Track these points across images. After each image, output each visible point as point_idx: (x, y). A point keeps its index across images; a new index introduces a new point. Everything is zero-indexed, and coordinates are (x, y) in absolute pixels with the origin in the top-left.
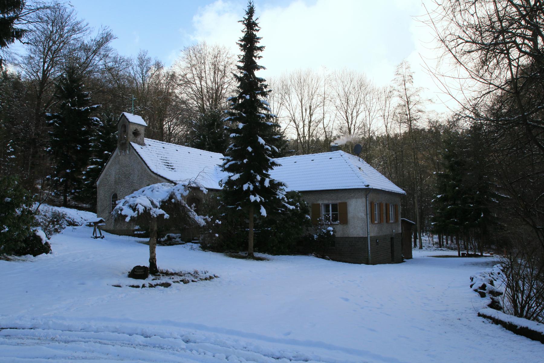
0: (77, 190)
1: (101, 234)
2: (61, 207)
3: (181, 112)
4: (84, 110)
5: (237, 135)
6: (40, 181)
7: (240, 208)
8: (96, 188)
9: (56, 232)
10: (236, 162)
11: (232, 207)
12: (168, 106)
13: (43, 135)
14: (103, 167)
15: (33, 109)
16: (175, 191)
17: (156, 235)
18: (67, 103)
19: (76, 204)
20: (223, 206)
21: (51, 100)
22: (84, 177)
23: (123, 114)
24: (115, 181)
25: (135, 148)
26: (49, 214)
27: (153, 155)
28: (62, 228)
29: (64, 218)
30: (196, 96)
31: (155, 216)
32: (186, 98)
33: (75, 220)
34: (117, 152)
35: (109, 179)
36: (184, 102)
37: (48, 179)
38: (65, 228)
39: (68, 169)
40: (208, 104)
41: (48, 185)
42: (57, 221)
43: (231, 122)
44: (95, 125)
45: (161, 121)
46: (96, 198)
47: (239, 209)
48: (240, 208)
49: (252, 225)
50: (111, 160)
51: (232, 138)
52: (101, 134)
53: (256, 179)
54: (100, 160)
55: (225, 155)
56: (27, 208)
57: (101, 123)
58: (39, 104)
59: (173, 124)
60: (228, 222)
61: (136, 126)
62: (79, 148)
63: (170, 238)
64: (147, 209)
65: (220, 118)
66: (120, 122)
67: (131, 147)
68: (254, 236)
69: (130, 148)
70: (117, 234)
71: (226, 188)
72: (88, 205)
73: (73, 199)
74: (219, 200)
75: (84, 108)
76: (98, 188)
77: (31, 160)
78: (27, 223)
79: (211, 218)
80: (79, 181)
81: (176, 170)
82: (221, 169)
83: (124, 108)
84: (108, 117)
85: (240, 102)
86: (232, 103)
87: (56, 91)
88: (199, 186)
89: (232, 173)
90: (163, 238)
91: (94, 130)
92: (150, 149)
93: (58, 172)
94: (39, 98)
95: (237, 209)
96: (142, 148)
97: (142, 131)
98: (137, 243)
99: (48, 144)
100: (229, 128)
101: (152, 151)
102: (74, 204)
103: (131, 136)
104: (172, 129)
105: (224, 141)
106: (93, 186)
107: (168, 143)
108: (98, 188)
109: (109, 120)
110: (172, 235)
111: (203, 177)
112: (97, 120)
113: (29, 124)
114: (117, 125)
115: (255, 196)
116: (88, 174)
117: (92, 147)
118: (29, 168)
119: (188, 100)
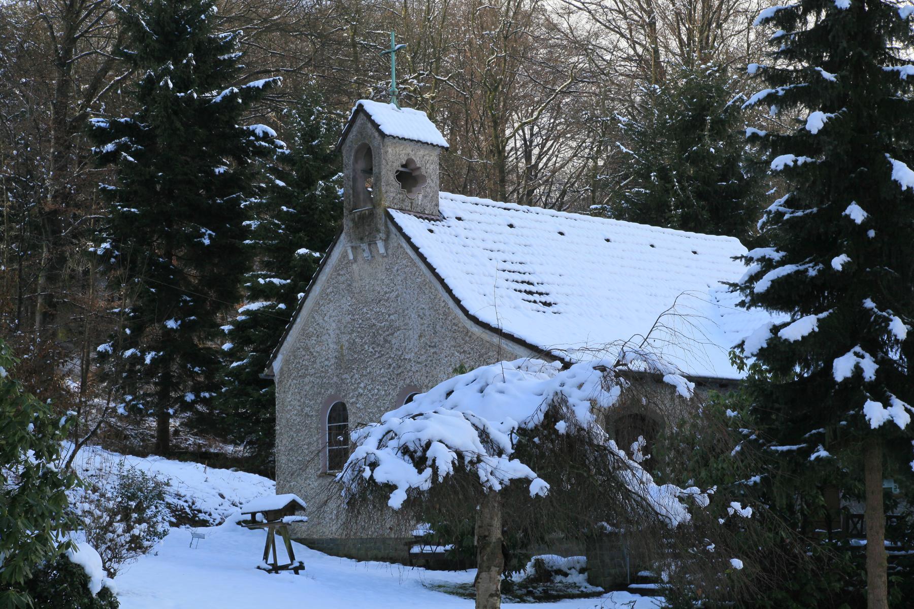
0: (202, 395)
1: (292, 557)
2: (150, 458)
3: (569, 86)
4: (219, 99)
5: (801, 160)
6: (75, 364)
7: (823, 453)
8: (270, 382)
9: (134, 549)
10: (802, 268)
11: (789, 451)
12: (521, 63)
13: (81, 197)
14: (294, 307)
15: (45, 104)
16: (566, 389)
17: (500, 559)
18: (160, 78)
19: (200, 446)
20: (751, 445)
21: (105, 70)
22: (227, 346)
23: (361, 106)
24: (340, 358)
25: (406, 230)
26: (110, 486)
27: (473, 256)
28: (156, 534)
29: (160, 496)
30: (626, 18)
31: (498, 487)
32: (588, 27)
33: (198, 505)
34: (342, 247)
35: (318, 349)
36: (581, 46)
37: (103, 356)
38: (165, 533)
39: (169, 318)
40: (674, 44)
41: (103, 377)
42: (140, 509)
43: (773, 107)
44: (261, 152)
45: (496, 124)
46: (273, 420)
47: (817, 458)
48: (823, 453)
49: (876, 522)
50: (323, 278)
51: (776, 173)
52: (281, 183)
53: (889, 333)
54: (283, 282)
55: (750, 246)
56: (38, 466)
57: (283, 143)
58: (64, 85)
59: (539, 132)
60: (773, 507)
61: (409, 150)
62: (207, 242)
63: (544, 574)
64: (467, 459)
65: (723, 95)
66: (351, 136)
67: (393, 229)
68: (889, 568)
69: (388, 234)
70: (350, 557)
71: (761, 372)
72: (241, 448)
73: (189, 425)
74: (735, 423)
75: (219, 94)
76: (280, 382)
77: (44, 290)
78: (36, 518)
79: (710, 496)
80: (210, 361)
81: (561, 310)
82: (738, 296)
83: (361, 84)
84: (307, 121)
85: (811, 25)
86: (780, 32)
87: (122, 34)
88: (660, 366)
89: (782, 314)
90: (518, 570)
91: (259, 173)
92: (464, 233)
93: (138, 330)
94: (63, 63)
95: (813, 457)
96: (431, 231)
97: (430, 166)
98: (425, 591)
99: (101, 231)
100: (767, 136)
101: (468, 242)
102: (195, 444)
103: (391, 189)
104: (536, 151)
105: (745, 188)
106: (261, 376)
107: (525, 207)
108: (280, 382)
109: (311, 133)
110: (552, 559)
111: (674, 332)
112: (266, 134)
113: (32, 160)
114: (339, 149)
115: (887, 404)
116: (241, 333)
117: (254, 234)
118: (38, 318)
119: (597, 35)
